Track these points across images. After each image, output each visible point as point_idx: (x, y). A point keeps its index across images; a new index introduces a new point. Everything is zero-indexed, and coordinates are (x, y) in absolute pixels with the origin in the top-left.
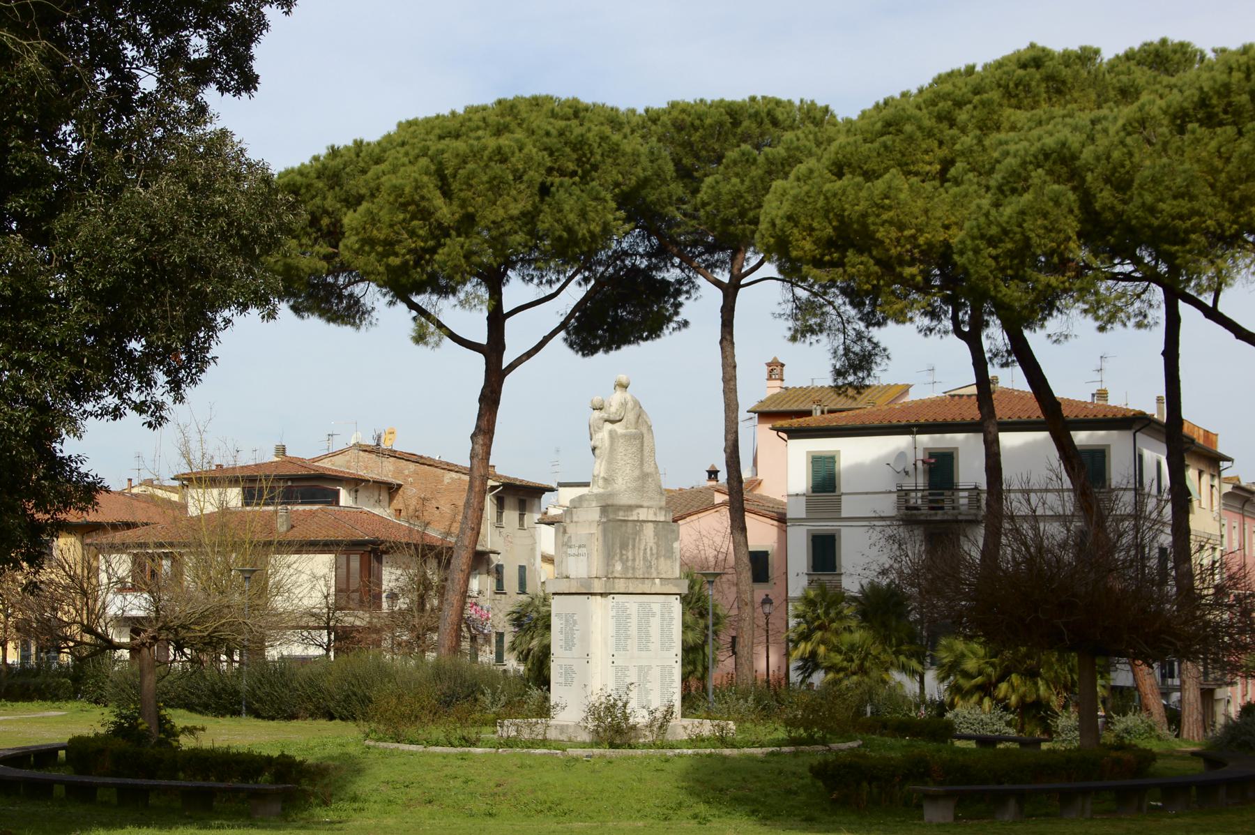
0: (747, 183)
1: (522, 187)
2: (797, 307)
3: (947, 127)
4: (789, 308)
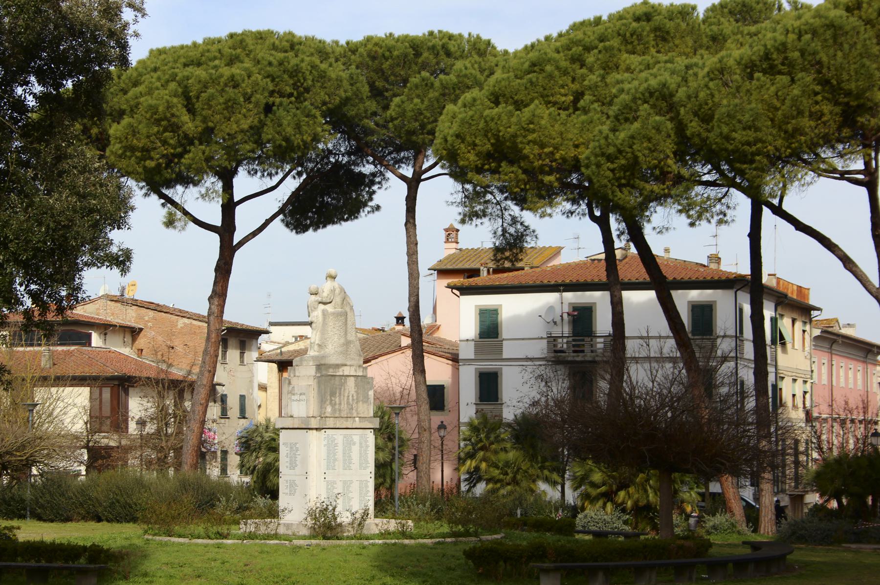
0: (426, 103)
1: (251, 106)
2: (466, 197)
3: (579, 67)
4: (459, 197)
